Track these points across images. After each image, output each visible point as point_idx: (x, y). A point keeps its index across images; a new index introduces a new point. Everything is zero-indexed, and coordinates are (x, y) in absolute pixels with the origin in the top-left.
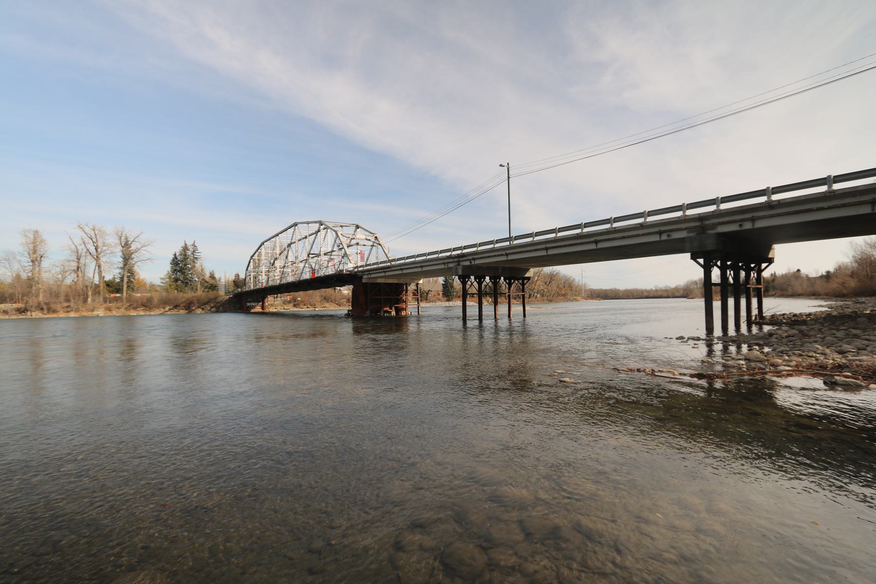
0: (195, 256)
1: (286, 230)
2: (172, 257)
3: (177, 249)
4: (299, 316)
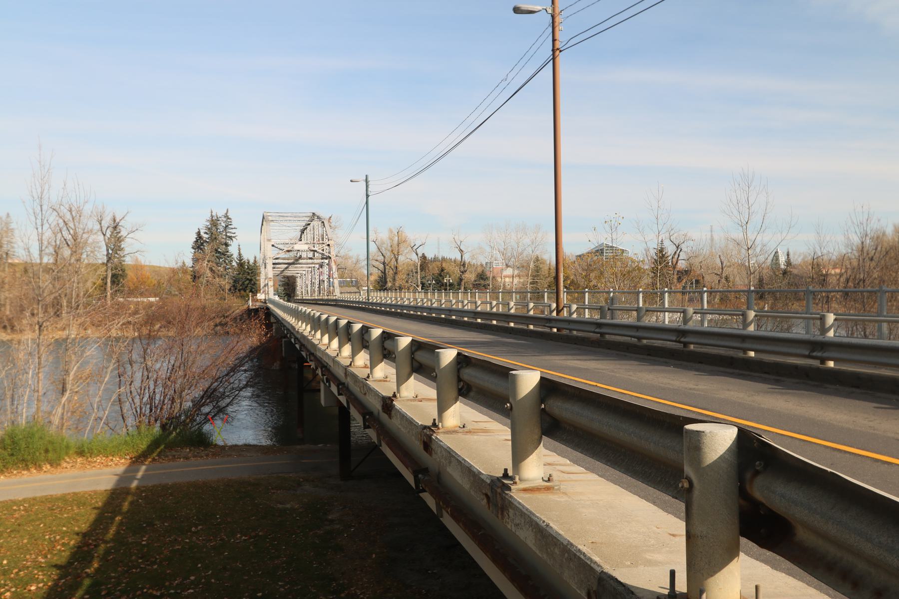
0: (228, 234)
1: (262, 225)
2: (194, 237)
3: (202, 223)
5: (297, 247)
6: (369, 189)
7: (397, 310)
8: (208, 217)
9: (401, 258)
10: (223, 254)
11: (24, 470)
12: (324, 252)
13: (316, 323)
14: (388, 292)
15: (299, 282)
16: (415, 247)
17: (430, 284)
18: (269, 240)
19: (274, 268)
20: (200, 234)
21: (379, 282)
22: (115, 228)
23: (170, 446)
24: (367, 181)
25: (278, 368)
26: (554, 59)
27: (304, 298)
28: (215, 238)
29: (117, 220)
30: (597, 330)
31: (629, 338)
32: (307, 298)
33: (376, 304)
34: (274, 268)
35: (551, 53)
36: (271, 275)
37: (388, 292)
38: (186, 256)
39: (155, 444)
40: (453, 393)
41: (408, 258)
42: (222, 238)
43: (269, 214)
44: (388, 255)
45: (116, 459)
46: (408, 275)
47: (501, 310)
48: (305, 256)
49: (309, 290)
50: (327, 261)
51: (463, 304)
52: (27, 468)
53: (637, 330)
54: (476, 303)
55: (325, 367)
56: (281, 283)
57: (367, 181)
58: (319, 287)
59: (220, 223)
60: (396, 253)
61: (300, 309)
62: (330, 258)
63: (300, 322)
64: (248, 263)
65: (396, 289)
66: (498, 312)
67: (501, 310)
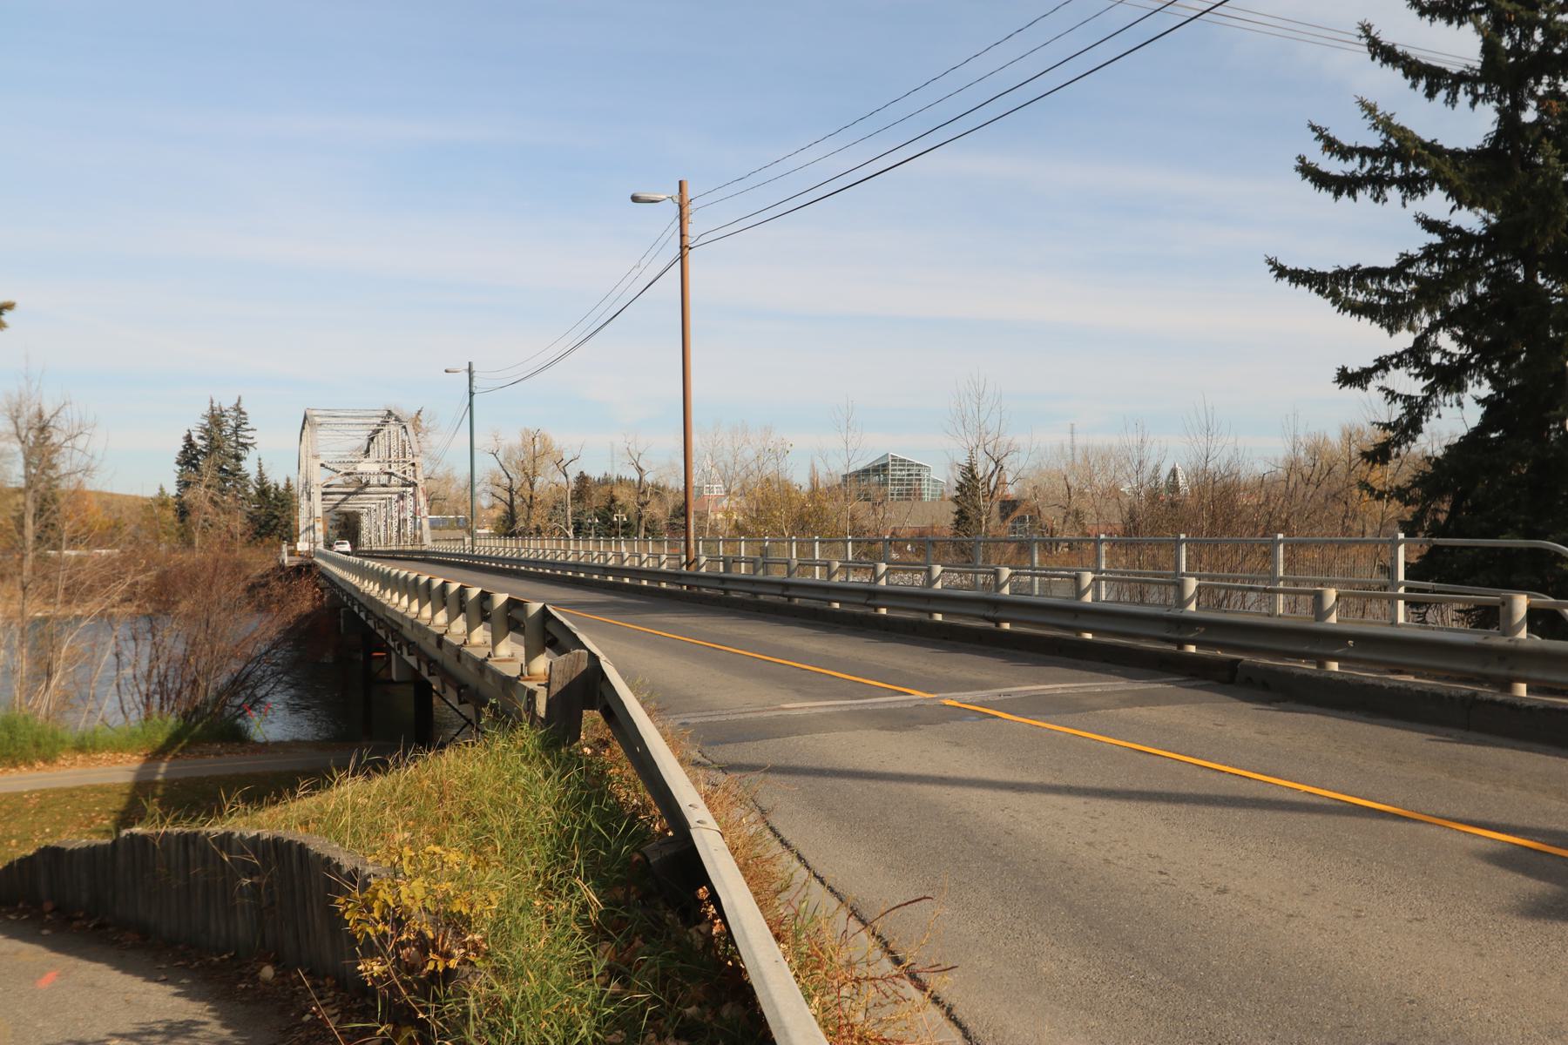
0: (241, 440)
1: (303, 428)
2: (179, 445)
3: (193, 421)
4: (1265, 686)
5: (361, 468)
6: (474, 384)
7: (555, 571)
8: (206, 410)
9: (539, 480)
10: (231, 474)
11: (11, 767)
12: (407, 476)
13: (387, 581)
14: (523, 540)
15: (365, 522)
16: (563, 463)
17: (590, 524)
18: (316, 457)
19: (323, 500)
20: (191, 440)
21: (504, 522)
22: (42, 429)
23: (196, 741)
24: (470, 371)
25: (331, 661)
26: (682, 257)
27: (374, 548)
28: (218, 447)
29: (47, 416)
30: (721, 586)
31: (776, 597)
32: (379, 549)
33: (484, 558)
34: (323, 500)
35: (679, 250)
36: (319, 512)
37: (523, 540)
39: (174, 739)
40: (478, 619)
41: (549, 481)
42: (229, 446)
43: (315, 413)
44: (518, 480)
45: (127, 756)
46: (555, 508)
47: (817, 577)
48: (376, 482)
49: (382, 536)
50: (410, 490)
51: (829, 571)
52: (15, 765)
53: (1076, 616)
54: (622, 556)
55: (395, 626)
56: (334, 524)
57: (470, 371)
58: (399, 530)
59: (227, 421)
60: (530, 472)
61: (366, 564)
62: (416, 485)
63: (366, 582)
64: (276, 489)
65: (531, 534)
66: (1098, 605)
67: (817, 577)
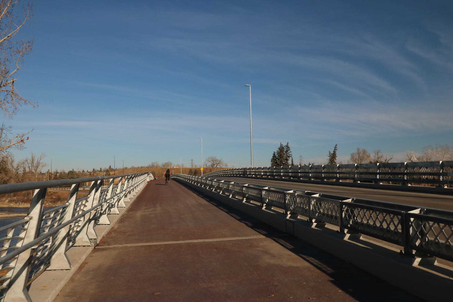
0: (288, 155)
38: (268, 164)
